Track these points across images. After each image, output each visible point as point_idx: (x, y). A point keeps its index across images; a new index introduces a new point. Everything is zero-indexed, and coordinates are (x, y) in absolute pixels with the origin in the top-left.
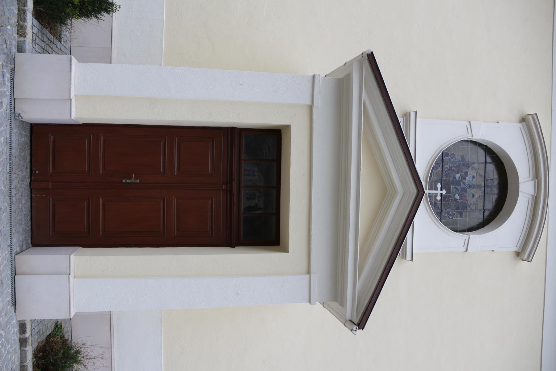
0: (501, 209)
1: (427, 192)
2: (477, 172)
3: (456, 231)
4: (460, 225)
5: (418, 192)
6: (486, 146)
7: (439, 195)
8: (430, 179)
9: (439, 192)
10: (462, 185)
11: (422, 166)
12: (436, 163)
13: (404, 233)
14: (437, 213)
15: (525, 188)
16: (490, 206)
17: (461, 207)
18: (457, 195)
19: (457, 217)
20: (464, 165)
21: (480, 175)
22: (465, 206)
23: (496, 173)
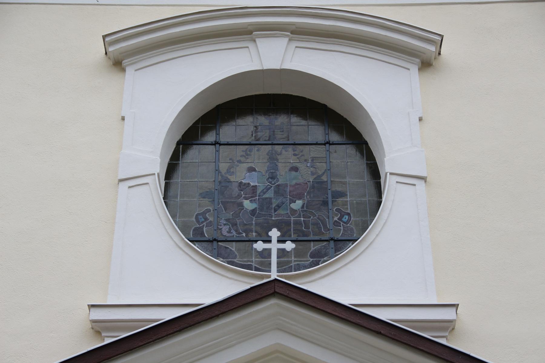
0: (325, 106)
1: (274, 275)
2: (240, 162)
3: (380, 203)
4: (365, 196)
5: (274, 294)
6: (178, 144)
7: (282, 246)
8: (257, 269)
9: (275, 245)
10: (270, 194)
11: (213, 285)
12: (218, 256)
13: (378, 327)
14: (338, 250)
15: (272, 55)
16: (316, 131)
17: (322, 194)
18: (293, 206)
19: (345, 203)
20: (223, 193)
21: (247, 155)
22: (319, 185)
23: (240, 122)
